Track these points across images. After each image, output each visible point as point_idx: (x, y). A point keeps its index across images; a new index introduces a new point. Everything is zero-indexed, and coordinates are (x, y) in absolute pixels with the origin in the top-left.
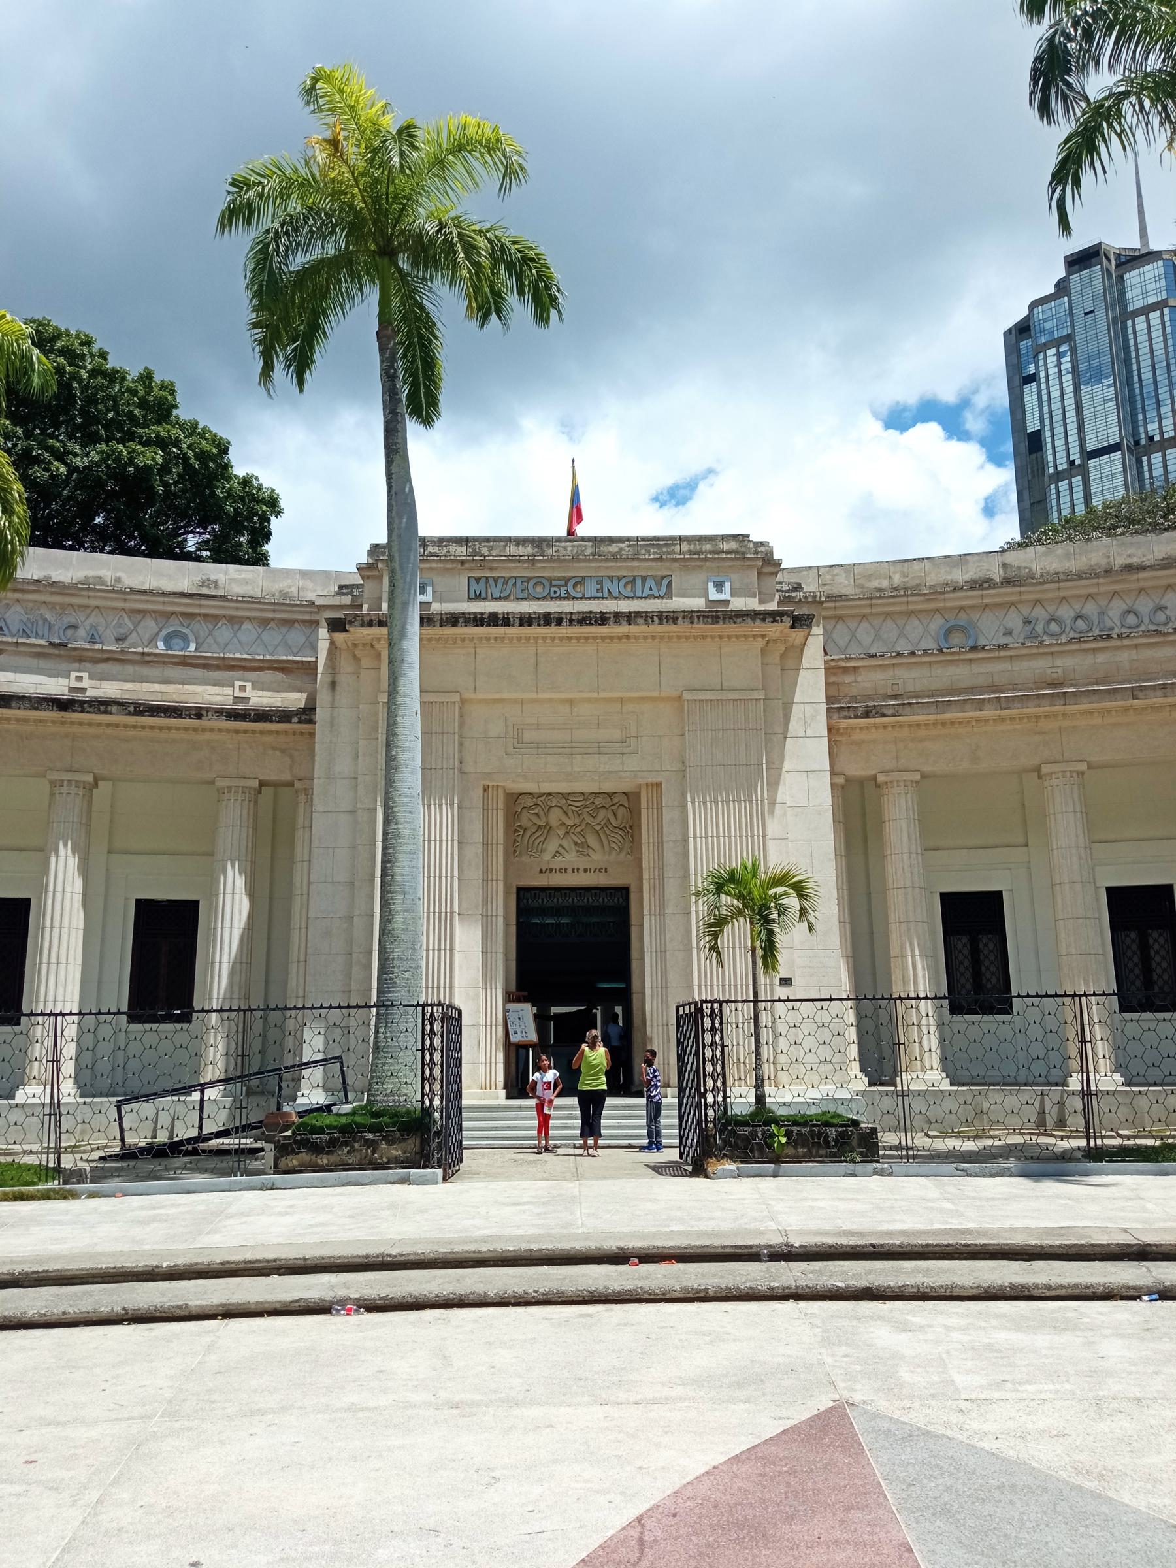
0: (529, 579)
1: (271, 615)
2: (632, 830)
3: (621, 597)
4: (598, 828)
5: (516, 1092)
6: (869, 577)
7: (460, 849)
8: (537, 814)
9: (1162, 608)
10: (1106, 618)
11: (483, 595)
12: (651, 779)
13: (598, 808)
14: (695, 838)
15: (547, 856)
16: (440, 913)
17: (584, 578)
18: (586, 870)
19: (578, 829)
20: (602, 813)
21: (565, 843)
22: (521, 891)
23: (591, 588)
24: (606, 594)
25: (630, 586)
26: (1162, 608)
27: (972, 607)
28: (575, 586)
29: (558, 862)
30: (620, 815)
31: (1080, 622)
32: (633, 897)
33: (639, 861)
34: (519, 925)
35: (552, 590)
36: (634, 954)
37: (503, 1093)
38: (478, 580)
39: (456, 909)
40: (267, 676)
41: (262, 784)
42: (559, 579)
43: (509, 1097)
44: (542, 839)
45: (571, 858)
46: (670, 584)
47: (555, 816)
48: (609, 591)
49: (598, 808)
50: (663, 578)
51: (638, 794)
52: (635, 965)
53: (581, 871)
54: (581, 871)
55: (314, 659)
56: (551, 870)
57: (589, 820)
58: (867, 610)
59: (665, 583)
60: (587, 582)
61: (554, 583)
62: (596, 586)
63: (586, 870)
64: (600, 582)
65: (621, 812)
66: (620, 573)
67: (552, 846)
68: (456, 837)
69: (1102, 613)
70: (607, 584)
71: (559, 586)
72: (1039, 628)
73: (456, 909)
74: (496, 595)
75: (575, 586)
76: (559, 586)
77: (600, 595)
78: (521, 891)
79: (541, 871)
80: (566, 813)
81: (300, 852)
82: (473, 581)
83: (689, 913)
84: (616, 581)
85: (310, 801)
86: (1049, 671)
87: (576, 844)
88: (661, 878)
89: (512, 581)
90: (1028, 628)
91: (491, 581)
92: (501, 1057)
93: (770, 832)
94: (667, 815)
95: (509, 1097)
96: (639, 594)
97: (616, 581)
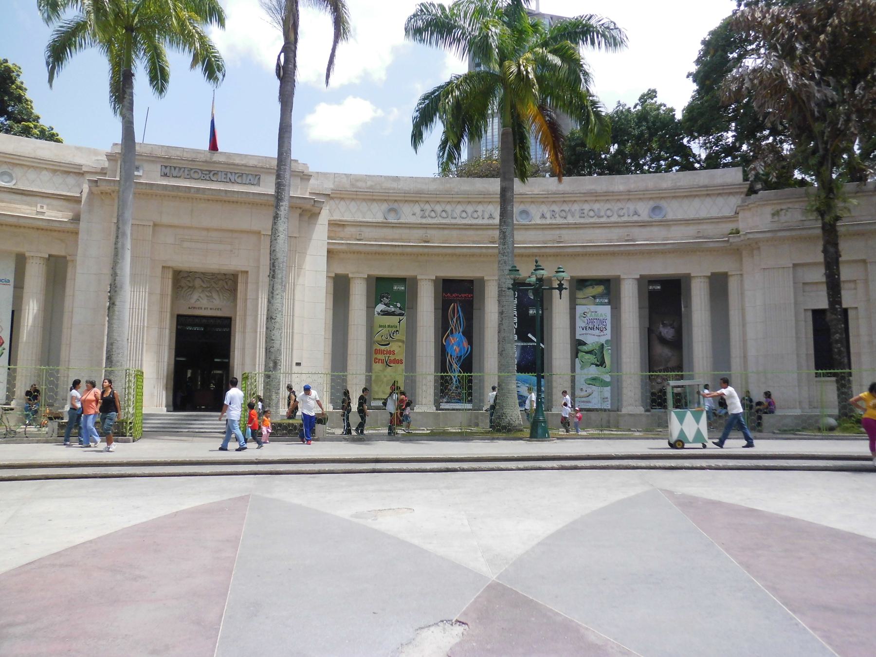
0: (192, 169)
1: (58, 168)
2: (233, 291)
3: (235, 182)
4: (218, 289)
5: (172, 409)
6: (357, 181)
7: (149, 296)
8: (189, 281)
9: (476, 211)
10: (454, 213)
11: (168, 175)
12: (243, 269)
13: (219, 280)
14: (144, 309)
15: (193, 301)
16: (138, 326)
17: (243, 174)
18: (211, 309)
19: (208, 289)
20: (221, 282)
21: (201, 295)
22: (179, 317)
23: (221, 177)
24: (228, 180)
25: (240, 178)
26: (476, 211)
27: (401, 201)
28: (214, 174)
29: (198, 305)
30: (229, 284)
31: (444, 213)
32: (233, 322)
33: (236, 306)
34: (177, 330)
35: (203, 175)
36: (232, 350)
37: (165, 409)
38: (166, 167)
39: (146, 325)
40: (55, 202)
41: (50, 255)
42: (206, 170)
43: (168, 411)
44: (190, 293)
45: (204, 302)
46: (259, 179)
47: (198, 283)
48: (230, 180)
49: (219, 280)
50: (256, 175)
51: (237, 275)
52: (231, 353)
53: (209, 309)
54: (209, 309)
55: (79, 195)
56: (194, 308)
57: (214, 285)
58: (355, 197)
59: (259, 177)
60: (220, 173)
61: (204, 172)
62: (224, 176)
63: (211, 309)
64: (226, 174)
65: (230, 282)
66: (236, 172)
67: (195, 296)
68: (146, 308)
69: (453, 211)
70: (229, 175)
71: (206, 174)
72: (427, 214)
73: (146, 325)
74: (174, 175)
75: (214, 174)
76: (206, 174)
77: (225, 180)
78: (179, 317)
79: (189, 308)
80: (203, 281)
81: (68, 291)
82: (163, 167)
83: (256, 332)
84: (233, 174)
85: (75, 267)
86: (424, 235)
87: (207, 296)
88: (245, 315)
89: (183, 169)
90: (422, 212)
91: (173, 168)
92: (164, 393)
93: (296, 298)
94: (250, 287)
95: (168, 411)
96: (244, 182)
97: (233, 174)
